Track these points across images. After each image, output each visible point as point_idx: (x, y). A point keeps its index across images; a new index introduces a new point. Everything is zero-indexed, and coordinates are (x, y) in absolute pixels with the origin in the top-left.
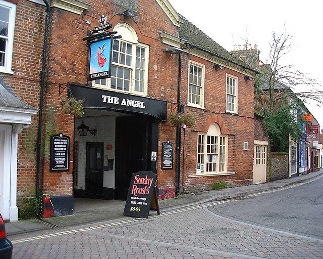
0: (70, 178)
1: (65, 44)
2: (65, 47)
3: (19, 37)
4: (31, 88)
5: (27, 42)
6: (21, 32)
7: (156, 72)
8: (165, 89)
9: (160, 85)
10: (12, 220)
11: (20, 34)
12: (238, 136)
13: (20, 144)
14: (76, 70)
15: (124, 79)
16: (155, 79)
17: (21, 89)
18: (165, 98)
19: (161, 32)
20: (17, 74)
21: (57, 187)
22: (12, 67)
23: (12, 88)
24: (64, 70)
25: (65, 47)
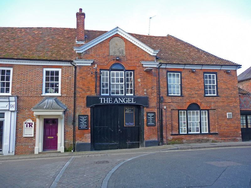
1: (83, 80)
7: (139, 82)
8: (147, 90)
9: (143, 88)
10: (61, 152)
22: (61, 93)
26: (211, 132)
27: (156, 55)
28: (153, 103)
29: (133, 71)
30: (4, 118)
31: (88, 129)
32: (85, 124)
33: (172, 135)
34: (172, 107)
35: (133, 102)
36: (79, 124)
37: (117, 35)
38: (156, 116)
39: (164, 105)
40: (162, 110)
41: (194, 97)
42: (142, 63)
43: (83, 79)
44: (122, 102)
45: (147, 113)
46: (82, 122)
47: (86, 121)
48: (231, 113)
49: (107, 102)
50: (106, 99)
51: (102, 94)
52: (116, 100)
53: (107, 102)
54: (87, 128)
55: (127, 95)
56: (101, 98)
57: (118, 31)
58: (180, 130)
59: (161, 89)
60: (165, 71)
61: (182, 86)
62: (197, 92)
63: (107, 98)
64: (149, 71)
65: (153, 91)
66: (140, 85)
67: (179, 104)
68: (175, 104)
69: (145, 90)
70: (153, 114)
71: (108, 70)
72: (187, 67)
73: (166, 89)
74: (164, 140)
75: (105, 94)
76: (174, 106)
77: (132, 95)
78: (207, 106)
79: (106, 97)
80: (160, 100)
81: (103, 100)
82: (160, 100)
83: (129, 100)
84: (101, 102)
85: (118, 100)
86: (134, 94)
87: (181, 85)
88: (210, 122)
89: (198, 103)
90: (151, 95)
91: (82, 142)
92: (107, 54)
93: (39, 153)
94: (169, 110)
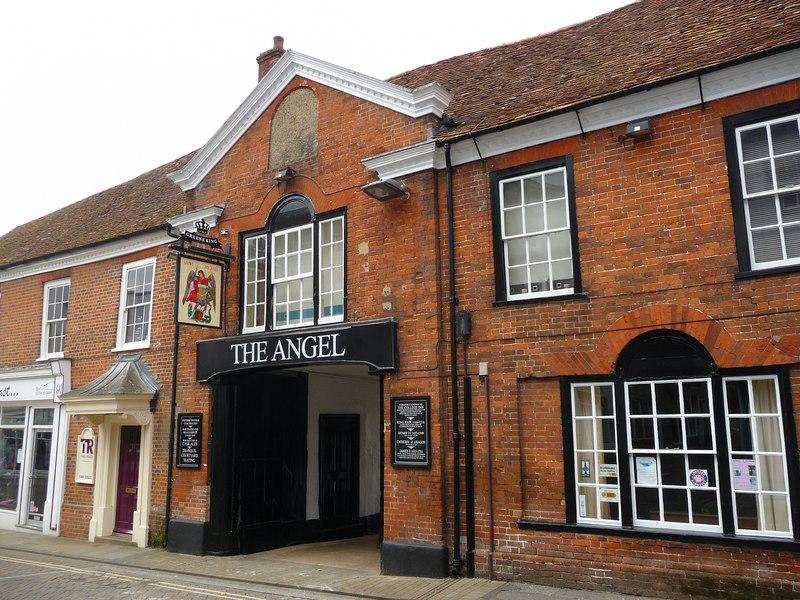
7: (364, 258)
8: (395, 286)
9: (380, 283)
28: (421, 349)
30: (788, 257)
31: (199, 468)
33: (524, 526)
34: (522, 367)
35: (335, 354)
37: (294, 85)
38: (435, 418)
39: (481, 357)
41: (655, 294)
42: (371, 166)
49: (253, 361)
52: (279, 350)
54: (199, 461)
57: (298, 65)
58: (580, 500)
59: (462, 270)
60: (479, 179)
61: (581, 235)
62: (676, 258)
63: (253, 344)
64: (394, 197)
67: (562, 343)
68: (536, 349)
69: (387, 289)
70: (417, 409)
72: (600, 119)
73: (489, 270)
76: (536, 357)
77: (262, 328)
78: (763, 348)
80: (459, 332)
82: (459, 332)
83: (321, 345)
84: (237, 362)
86: (267, 328)
87: (574, 230)
89: (690, 330)
90: (410, 312)
92: (261, 168)
93: (97, 539)
94: (508, 380)
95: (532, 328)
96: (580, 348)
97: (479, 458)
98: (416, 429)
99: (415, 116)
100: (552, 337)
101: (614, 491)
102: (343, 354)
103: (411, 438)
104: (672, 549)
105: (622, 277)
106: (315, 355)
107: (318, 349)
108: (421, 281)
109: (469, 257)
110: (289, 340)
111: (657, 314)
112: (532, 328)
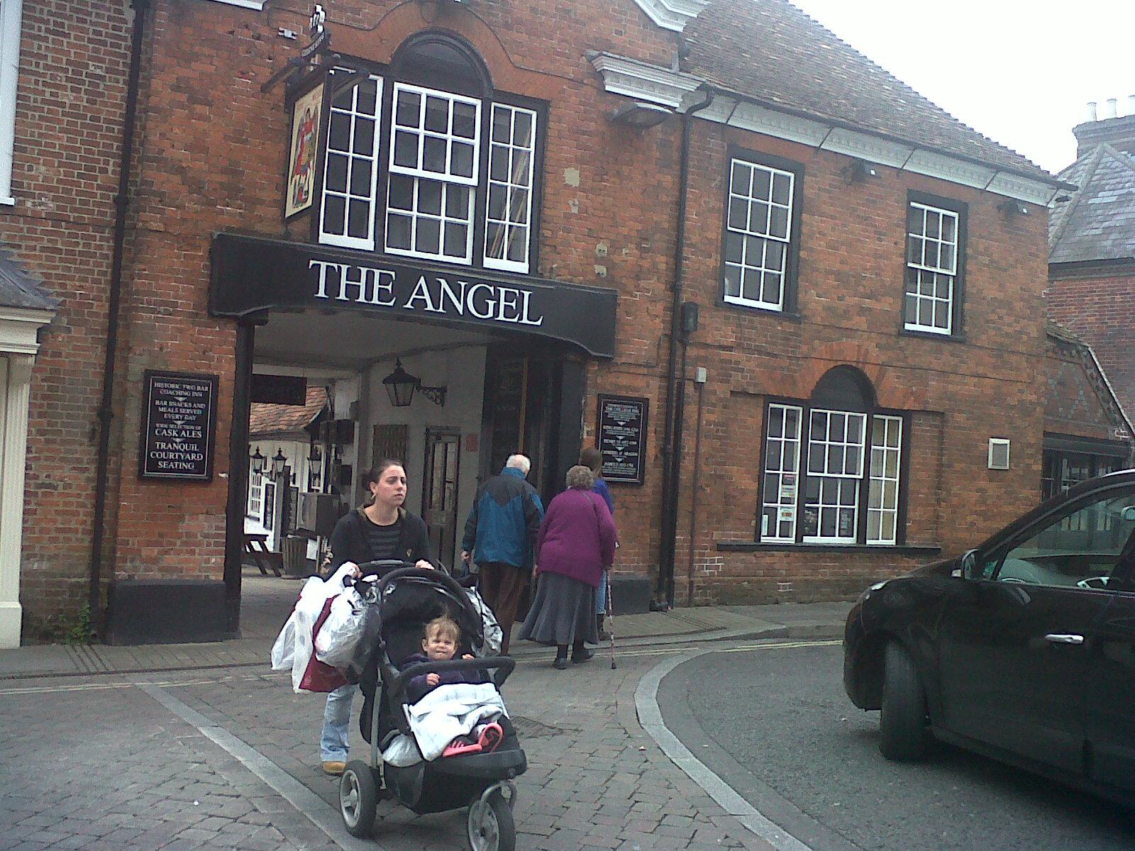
0: (217, 528)
1: (199, 108)
2: (201, 118)
3: (36, 92)
4: (80, 248)
5: (63, 105)
6: (44, 75)
8: (615, 247)
9: (593, 235)
11: (40, 47)
12: (960, 418)
13: (41, 415)
14: (240, 190)
15: (443, 218)
16: (568, 216)
17: (43, 249)
18: (610, 279)
19: (595, 53)
20: (29, 204)
21: (166, 552)
23: (13, 246)
24: (196, 186)
25: (201, 118)
26: (911, 543)
27: (680, 29)
29: (542, 106)
32: (187, 441)
35: (525, 321)
36: (148, 438)
40: (681, 386)
43: (193, 100)
44: (460, 308)
45: (605, 399)
46: (170, 421)
47: (200, 421)
48: (1007, 442)
49: (362, 299)
50: (353, 275)
51: (325, 238)
52: (420, 292)
53: (362, 299)
55: (489, 263)
56: (323, 265)
59: (686, 252)
60: (716, 144)
65: (646, 264)
66: (575, 210)
68: (750, 363)
69: (602, 246)
70: (631, 412)
71: (379, 68)
74: (681, 578)
75: (344, 241)
79: (354, 258)
81: (333, 276)
83: (502, 303)
85: (434, 289)
88: (911, 486)
90: (630, 287)
91: (159, 575)
94: (722, 390)
95: (750, 340)
96: (789, 370)
97: (684, 477)
98: (627, 438)
99: (660, 23)
100: (768, 354)
101: (791, 511)
102: (539, 323)
103: (620, 449)
104: (835, 559)
105: (828, 309)
106: (490, 314)
107: (497, 307)
108: (647, 250)
109: (695, 238)
110: (443, 281)
111: (848, 350)
112: (750, 340)
